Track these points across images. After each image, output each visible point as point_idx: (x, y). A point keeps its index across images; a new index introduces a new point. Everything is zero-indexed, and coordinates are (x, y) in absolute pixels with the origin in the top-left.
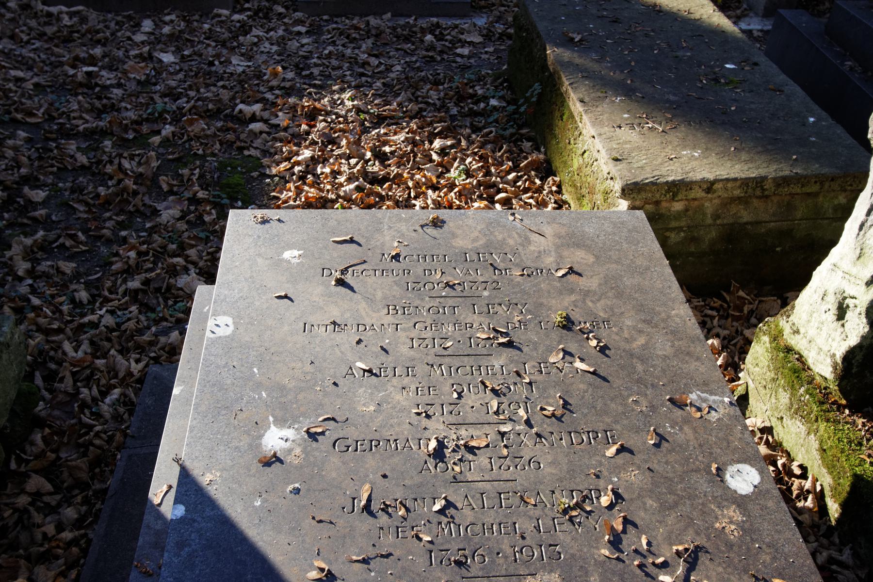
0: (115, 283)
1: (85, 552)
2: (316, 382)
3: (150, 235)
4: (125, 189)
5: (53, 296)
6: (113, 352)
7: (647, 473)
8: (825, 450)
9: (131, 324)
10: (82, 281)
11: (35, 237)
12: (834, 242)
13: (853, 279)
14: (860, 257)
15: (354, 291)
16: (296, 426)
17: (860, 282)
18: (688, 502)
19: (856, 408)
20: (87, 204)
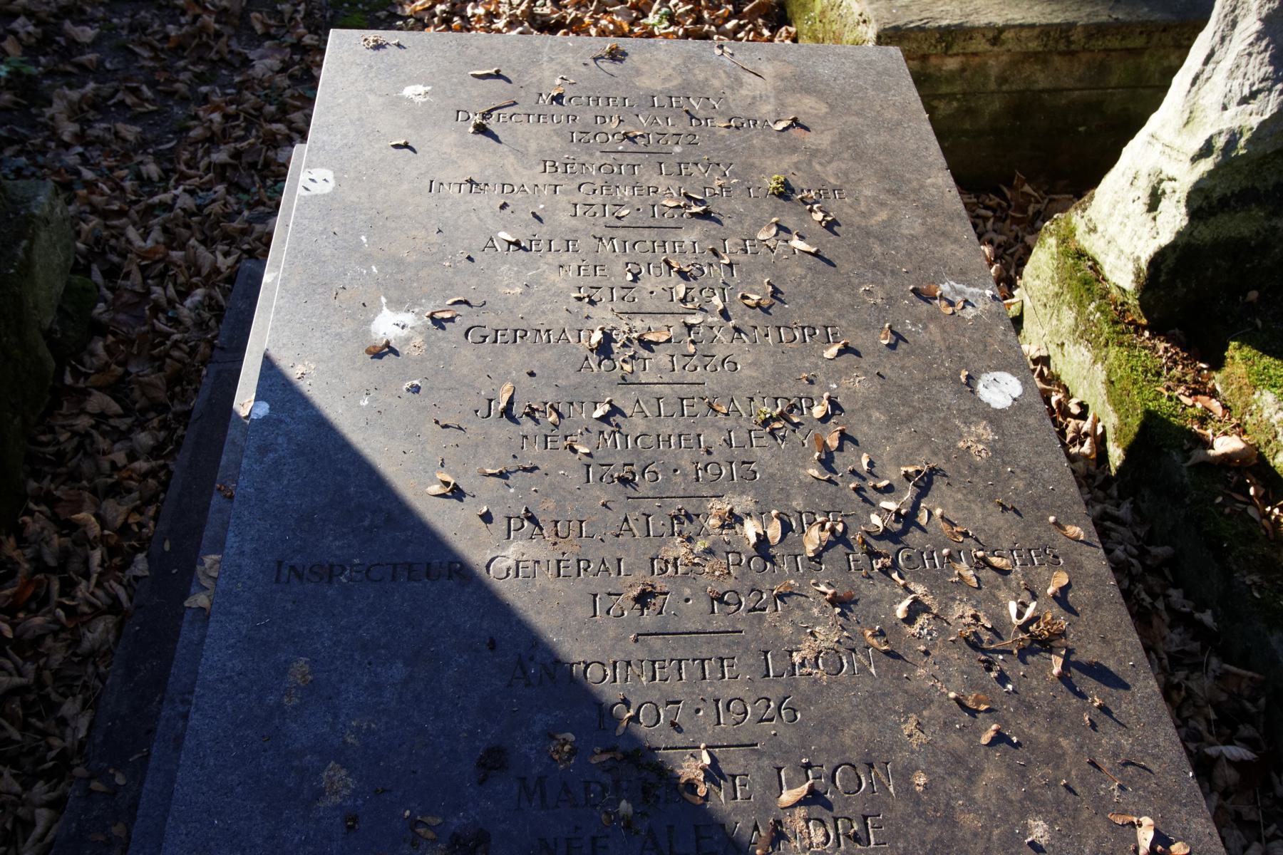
0: (194, 154)
1: (165, 486)
2: (445, 255)
3: (239, 92)
4: (204, 28)
5: (111, 169)
6: (193, 242)
7: (876, 379)
8: (1112, 382)
9: (216, 207)
10: (151, 151)
11: (83, 91)
12: (1155, 105)
13: (1174, 154)
14: (1188, 123)
15: (499, 142)
16: (417, 310)
17: (1182, 157)
18: (925, 416)
19: (1158, 330)
20: (153, 48)
